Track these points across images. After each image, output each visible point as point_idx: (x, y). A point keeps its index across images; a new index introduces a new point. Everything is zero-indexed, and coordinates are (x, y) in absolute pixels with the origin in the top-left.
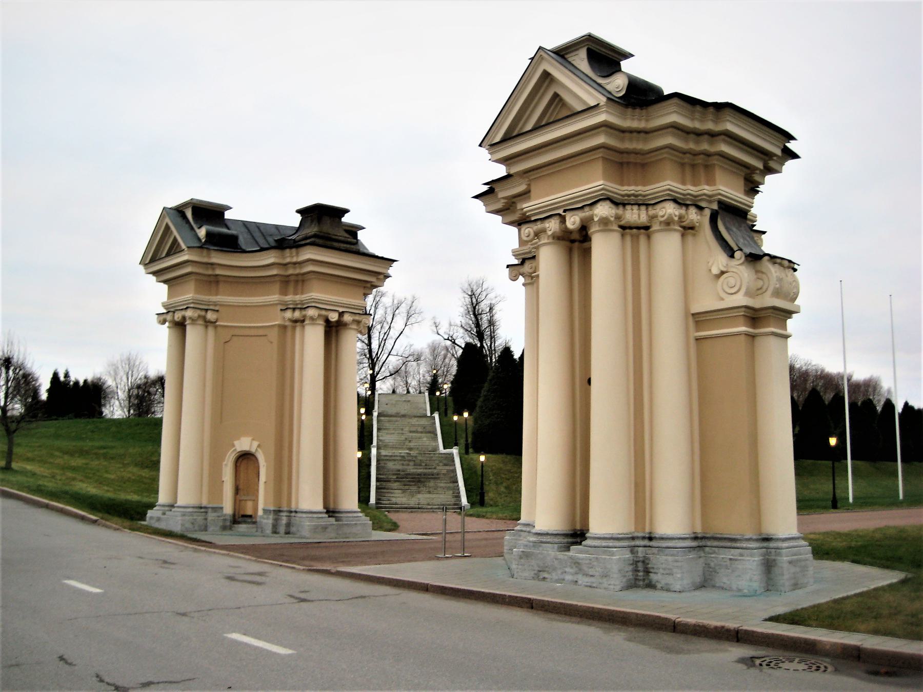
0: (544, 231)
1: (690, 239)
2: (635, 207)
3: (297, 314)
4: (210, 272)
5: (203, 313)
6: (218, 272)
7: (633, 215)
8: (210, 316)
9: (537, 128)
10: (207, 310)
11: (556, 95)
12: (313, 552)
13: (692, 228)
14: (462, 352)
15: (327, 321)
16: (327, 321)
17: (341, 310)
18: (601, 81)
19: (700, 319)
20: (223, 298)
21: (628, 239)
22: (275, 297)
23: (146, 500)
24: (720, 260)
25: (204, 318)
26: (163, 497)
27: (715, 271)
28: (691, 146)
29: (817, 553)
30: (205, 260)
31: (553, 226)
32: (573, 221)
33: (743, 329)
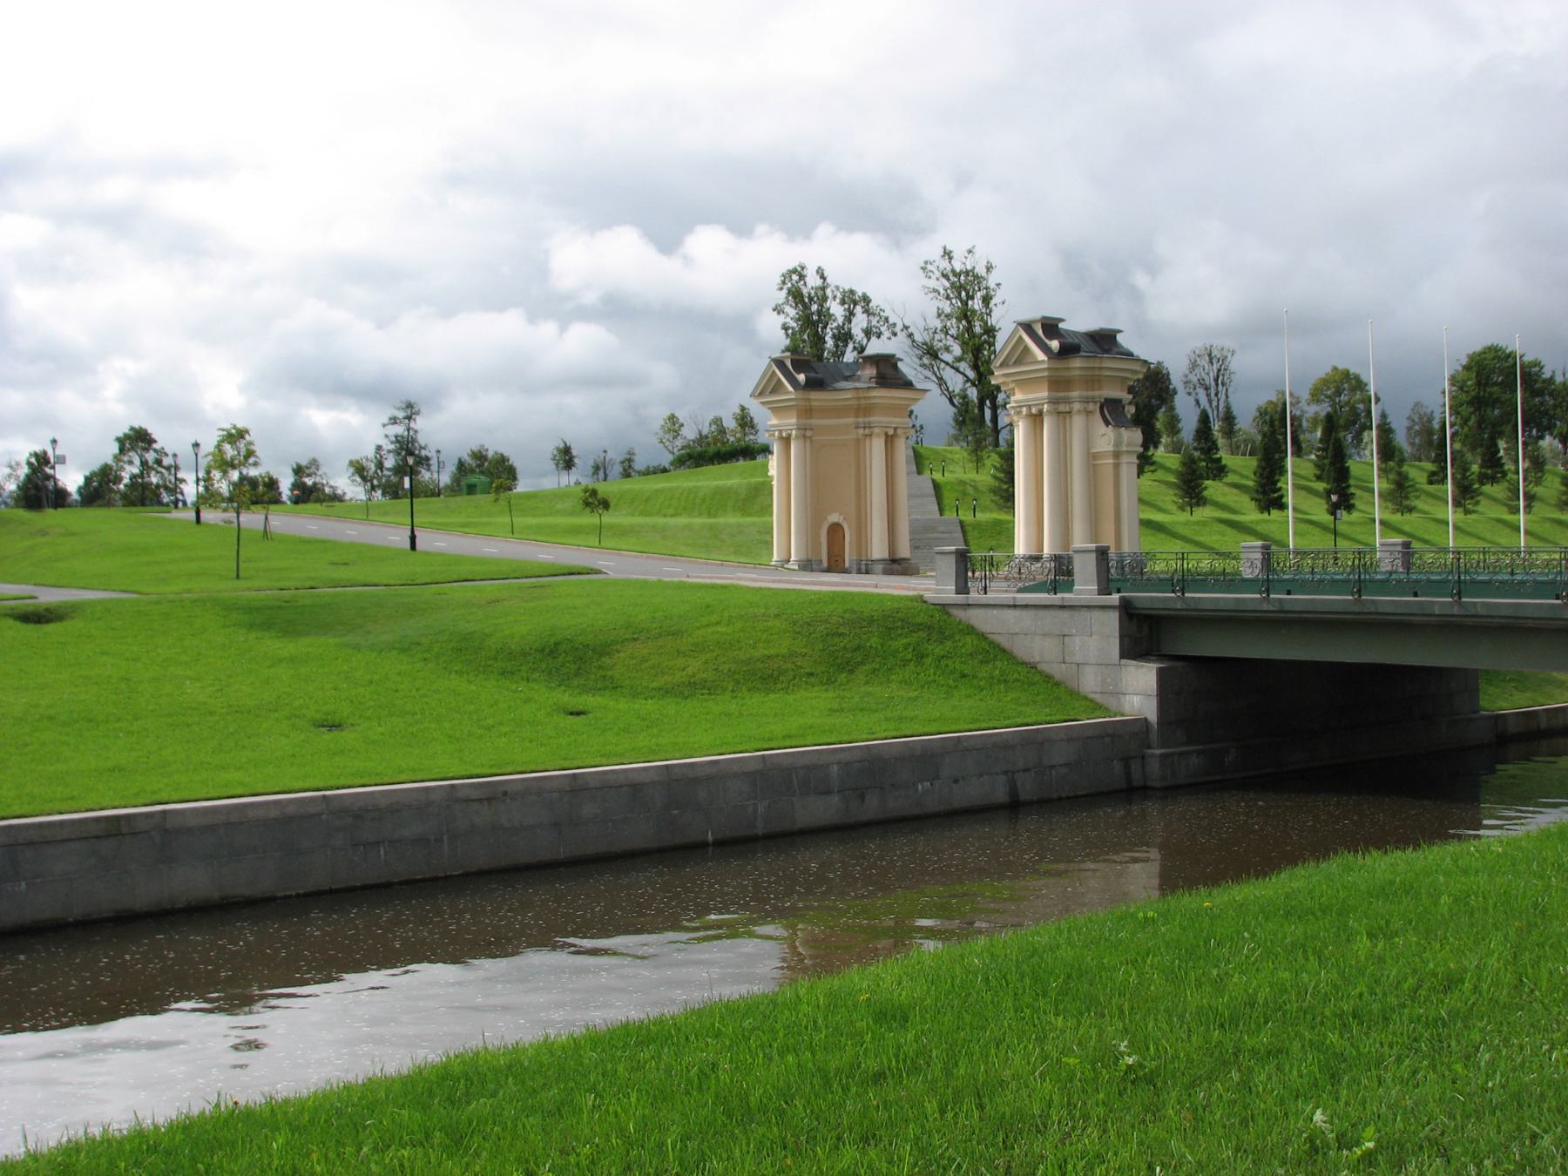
3: (867, 431)
7: (1062, 408)
13: (1091, 412)
15: (886, 434)
16: (886, 434)
18: (1047, 341)
20: (815, 422)
21: (1061, 419)
22: (851, 420)
27: (1100, 433)
32: (1034, 411)
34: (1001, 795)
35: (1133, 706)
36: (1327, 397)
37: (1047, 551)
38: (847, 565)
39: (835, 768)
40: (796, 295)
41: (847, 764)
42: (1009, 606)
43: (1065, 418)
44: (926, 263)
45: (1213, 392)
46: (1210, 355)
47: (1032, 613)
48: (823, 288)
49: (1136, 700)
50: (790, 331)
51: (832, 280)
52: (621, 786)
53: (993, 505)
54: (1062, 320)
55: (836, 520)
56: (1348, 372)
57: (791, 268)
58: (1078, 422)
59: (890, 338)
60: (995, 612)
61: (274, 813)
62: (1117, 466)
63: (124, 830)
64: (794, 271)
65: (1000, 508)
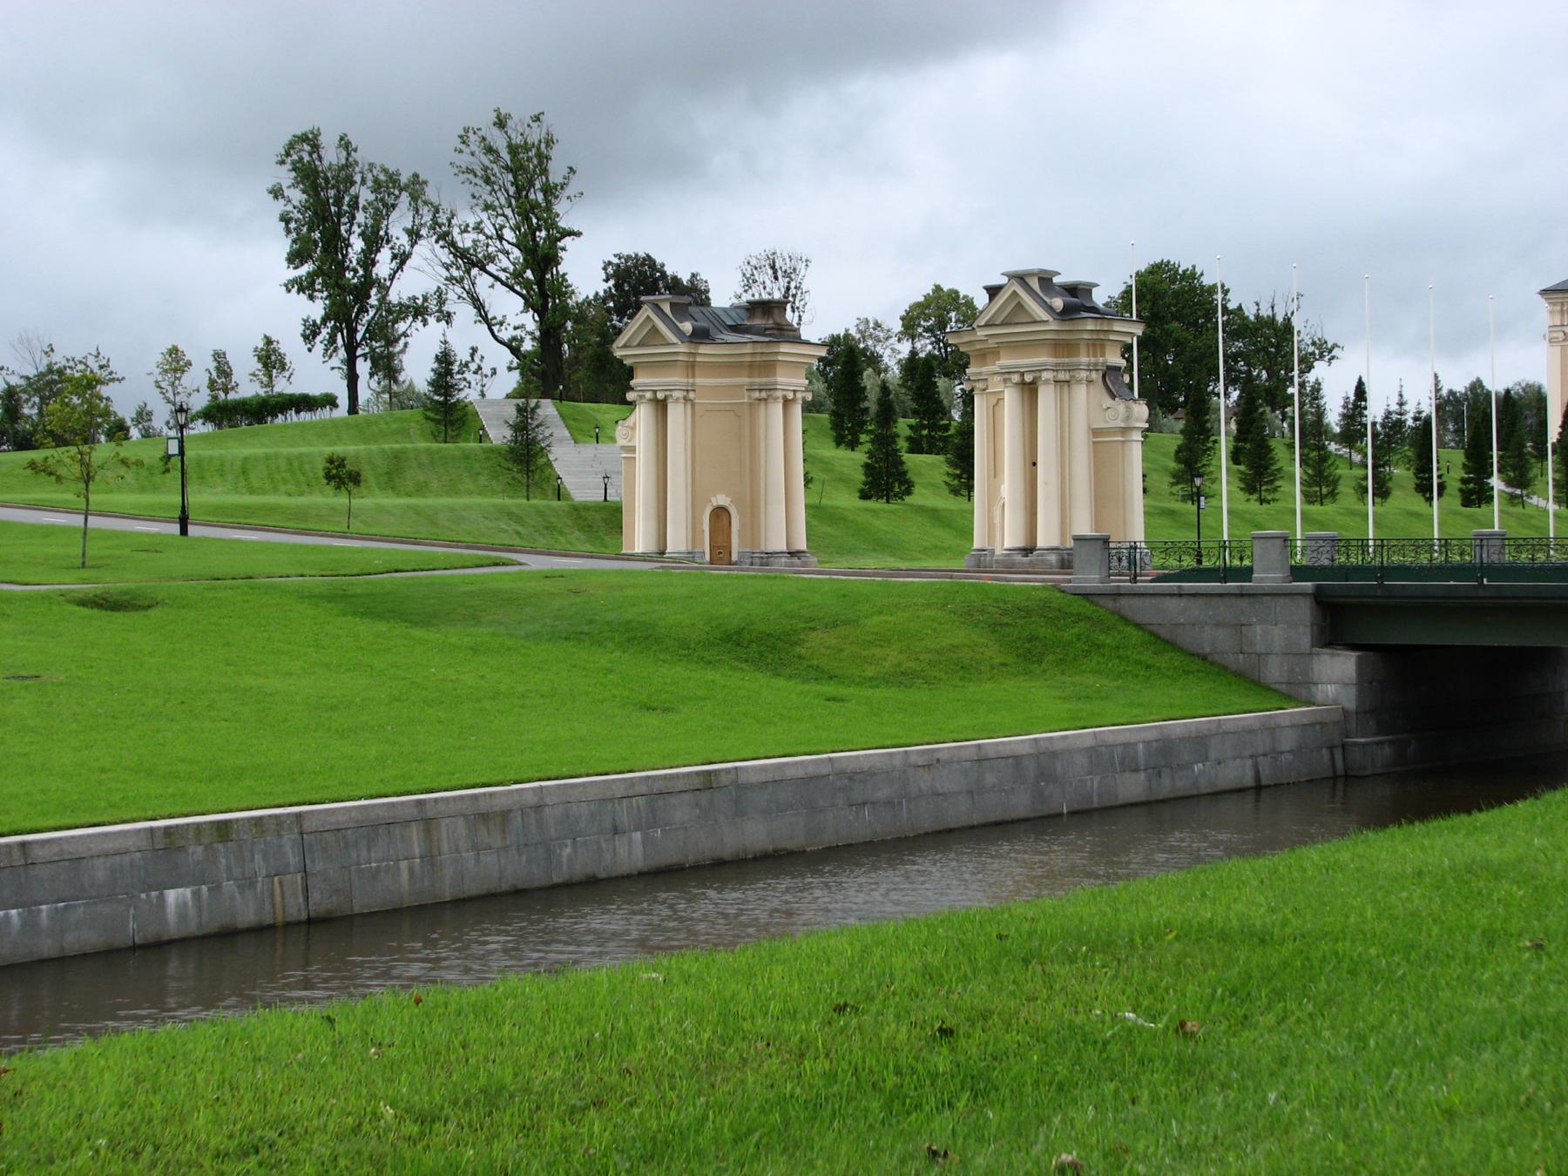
0: (1010, 379)
1: (1091, 387)
3: (764, 394)
5: (685, 393)
8: (691, 395)
9: (1003, 324)
10: (688, 391)
11: (1019, 303)
12: (1133, 562)
19: (1096, 432)
24: (1108, 401)
27: (1104, 407)
28: (1094, 337)
29: (396, 457)
31: (1016, 378)
32: (1028, 378)
34: (1249, 780)
35: (1327, 696)
36: (927, 330)
37: (1041, 543)
38: (734, 557)
39: (1141, 746)
40: (308, 176)
41: (1148, 742)
42: (1172, 595)
44: (466, 130)
46: (773, 267)
47: (1200, 601)
48: (347, 166)
49: (1331, 689)
50: (293, 225)
51: (362, 156)
52: (1008, 757)
53: (944, 485)
55: (721, 503)
56: (957, 292)
57: (299, 133)
60: (1153, 601)
61: (801, 773)
63: (714, 786)
64: (304, 138)
65: (955, 492)
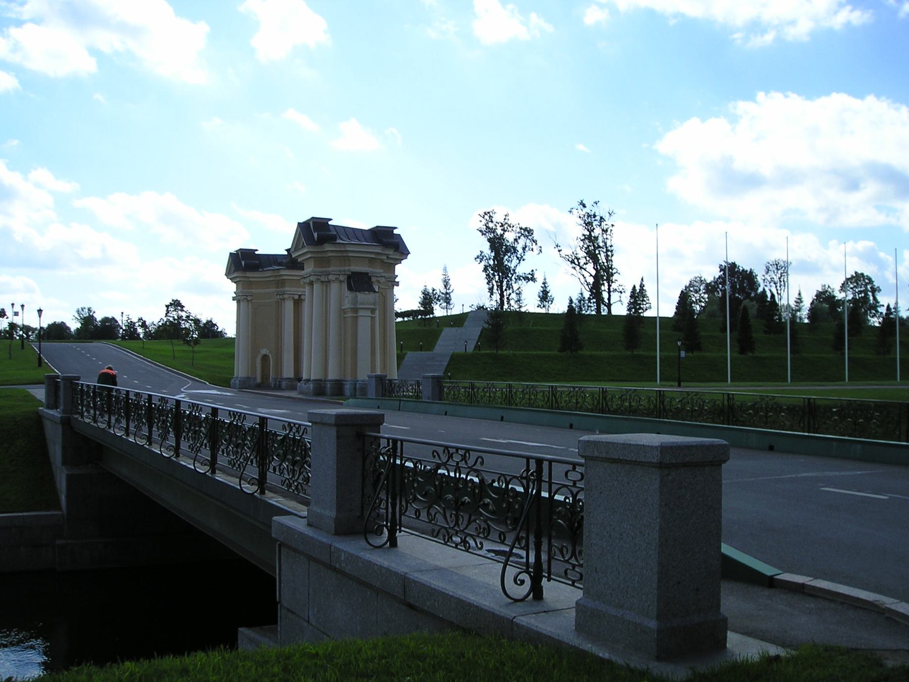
2: (324, 276)
4: (247, 280)
5: (245, 297)
6: (251, 279)
8: (249, 298)
10: (339, 275)
14: (394, 307)
17: (300, 294)
22: (273, 290)
23: (231, 376)
25: (247, 299)
26: (235, 375)
30: (244, 275)
33: (350, 315)
43: (327, 286)
45: (778, 285)
54: (330, 220)
55: (265, 353)
58: (334, 287)
59: (560, 246)
62: (356, 318)
